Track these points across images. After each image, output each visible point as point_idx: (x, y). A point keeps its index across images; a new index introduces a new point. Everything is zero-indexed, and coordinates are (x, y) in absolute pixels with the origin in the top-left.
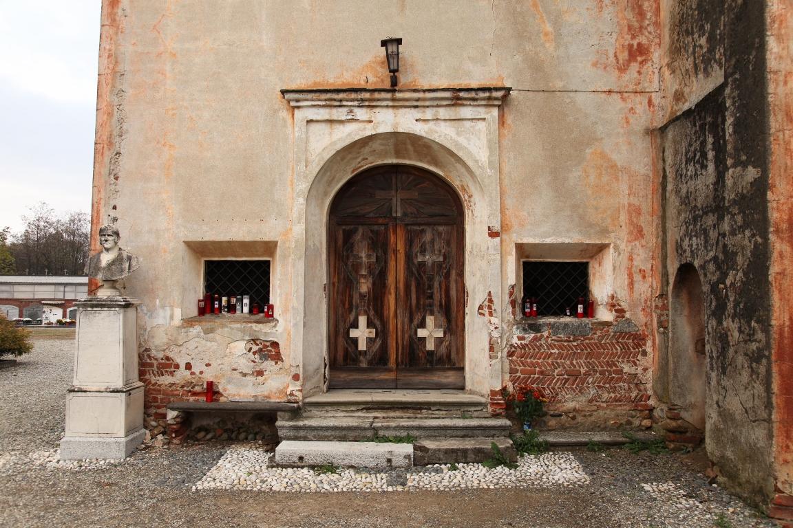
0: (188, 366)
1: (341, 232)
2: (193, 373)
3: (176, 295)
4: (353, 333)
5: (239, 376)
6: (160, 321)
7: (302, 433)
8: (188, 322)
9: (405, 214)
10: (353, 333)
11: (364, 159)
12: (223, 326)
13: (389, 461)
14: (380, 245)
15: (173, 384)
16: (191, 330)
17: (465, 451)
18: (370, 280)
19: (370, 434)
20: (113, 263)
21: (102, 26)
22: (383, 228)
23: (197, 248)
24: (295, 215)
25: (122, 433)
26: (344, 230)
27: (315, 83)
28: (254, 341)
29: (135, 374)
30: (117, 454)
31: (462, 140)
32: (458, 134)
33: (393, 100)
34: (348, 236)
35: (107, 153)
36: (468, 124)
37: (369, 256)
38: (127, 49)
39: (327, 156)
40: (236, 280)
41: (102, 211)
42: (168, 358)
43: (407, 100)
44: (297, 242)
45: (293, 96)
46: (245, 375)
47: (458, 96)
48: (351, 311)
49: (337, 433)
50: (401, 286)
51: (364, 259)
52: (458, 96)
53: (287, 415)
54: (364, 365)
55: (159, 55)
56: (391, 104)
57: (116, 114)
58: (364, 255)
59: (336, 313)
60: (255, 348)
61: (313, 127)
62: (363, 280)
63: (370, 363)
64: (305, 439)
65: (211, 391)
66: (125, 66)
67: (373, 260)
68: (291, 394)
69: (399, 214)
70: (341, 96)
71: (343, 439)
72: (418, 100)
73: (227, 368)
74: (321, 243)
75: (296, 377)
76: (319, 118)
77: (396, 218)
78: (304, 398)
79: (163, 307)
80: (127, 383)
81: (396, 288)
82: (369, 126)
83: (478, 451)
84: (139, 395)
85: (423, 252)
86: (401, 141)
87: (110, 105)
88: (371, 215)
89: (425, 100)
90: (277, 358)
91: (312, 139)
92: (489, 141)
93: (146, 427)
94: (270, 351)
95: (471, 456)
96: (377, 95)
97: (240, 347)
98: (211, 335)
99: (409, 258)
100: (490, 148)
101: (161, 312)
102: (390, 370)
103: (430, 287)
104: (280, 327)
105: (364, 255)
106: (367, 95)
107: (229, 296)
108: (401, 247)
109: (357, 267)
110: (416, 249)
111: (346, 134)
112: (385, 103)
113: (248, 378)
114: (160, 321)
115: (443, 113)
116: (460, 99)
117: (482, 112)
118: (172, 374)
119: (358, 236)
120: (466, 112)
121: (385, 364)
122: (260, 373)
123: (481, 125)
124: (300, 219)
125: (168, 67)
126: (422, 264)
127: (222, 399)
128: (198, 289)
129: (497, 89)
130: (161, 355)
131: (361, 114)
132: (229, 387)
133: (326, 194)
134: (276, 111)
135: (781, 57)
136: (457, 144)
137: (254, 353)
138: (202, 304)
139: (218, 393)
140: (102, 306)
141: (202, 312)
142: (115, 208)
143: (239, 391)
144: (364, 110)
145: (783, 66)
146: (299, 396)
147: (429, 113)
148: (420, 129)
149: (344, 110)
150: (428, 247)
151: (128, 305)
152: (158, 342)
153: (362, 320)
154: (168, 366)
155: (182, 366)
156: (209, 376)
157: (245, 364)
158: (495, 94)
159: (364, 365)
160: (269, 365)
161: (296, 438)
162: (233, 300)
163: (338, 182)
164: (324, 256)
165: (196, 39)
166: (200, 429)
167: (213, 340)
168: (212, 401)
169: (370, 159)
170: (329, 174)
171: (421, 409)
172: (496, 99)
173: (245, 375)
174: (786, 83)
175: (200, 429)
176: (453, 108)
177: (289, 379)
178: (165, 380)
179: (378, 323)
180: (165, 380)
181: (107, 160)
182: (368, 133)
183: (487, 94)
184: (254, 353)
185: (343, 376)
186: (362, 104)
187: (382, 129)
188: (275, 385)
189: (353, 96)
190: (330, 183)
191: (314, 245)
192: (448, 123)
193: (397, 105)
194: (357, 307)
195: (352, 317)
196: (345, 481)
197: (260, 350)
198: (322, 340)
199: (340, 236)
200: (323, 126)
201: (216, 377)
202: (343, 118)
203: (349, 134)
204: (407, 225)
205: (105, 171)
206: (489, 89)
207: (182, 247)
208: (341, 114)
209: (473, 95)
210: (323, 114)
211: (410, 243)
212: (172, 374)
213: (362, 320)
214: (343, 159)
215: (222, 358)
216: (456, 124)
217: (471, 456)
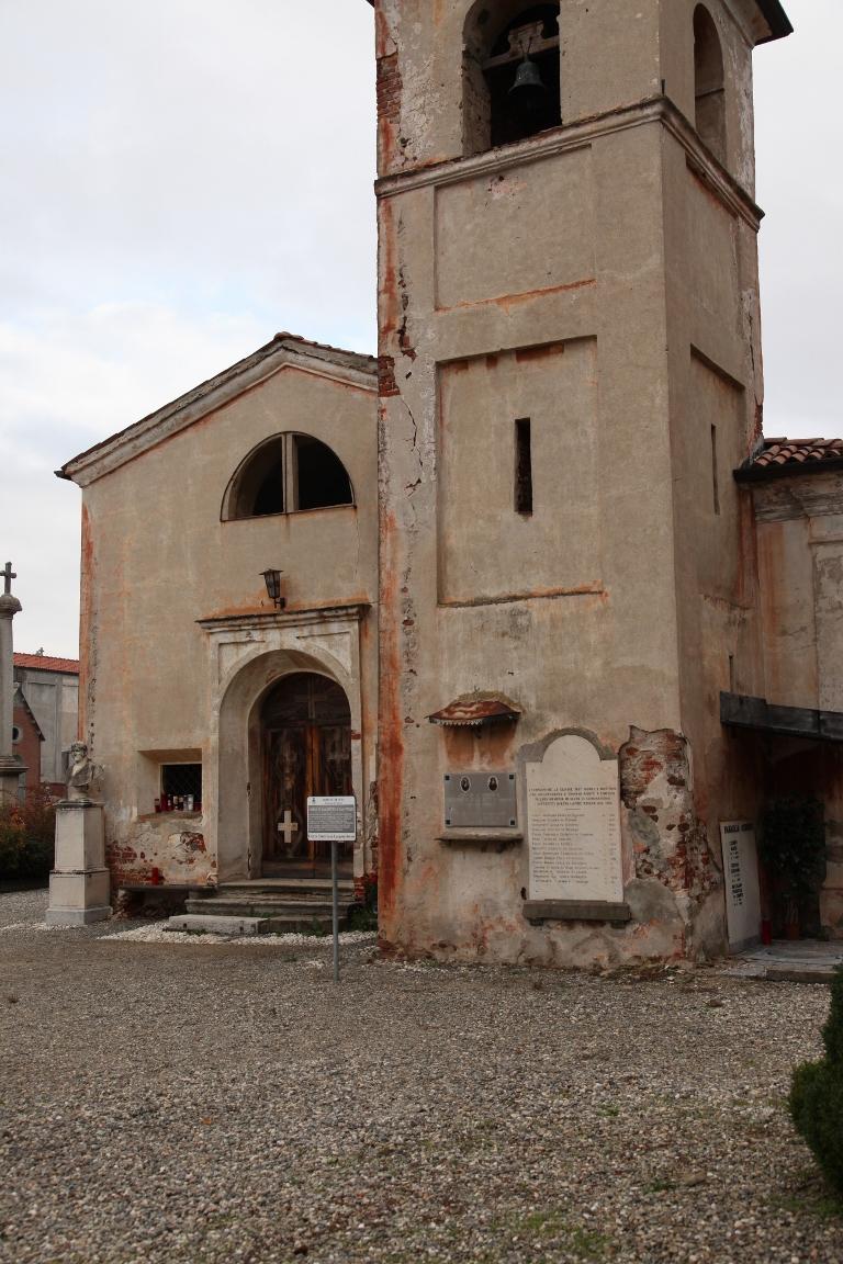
0: (143, 855)
1: (270, 735)
2: (145, 861)
3: (134, 797)
4: (281, 827)
5: (176, 863)
6: (123, 817)
7: (202, 909)
8: (142, 818)
9: (319, 716)
10: (281, 827)
11: (272, 671)
12: (164, 821)
13: (242, 929)
14: (300, 746)
15: (133, 870)
16: (143, 825)
17: (294, 923)
18: (294, 776)
19: (248, 910)
20: (80, 772)
21: (82, 574)
22: (302, 730)
23: (151, 756)
24: (212, 727)
25: (83, 906)
26: (272, 734)
27: (226, 611)
28: (187, 833)
29: (101, 860)
30: (79, 922)
31: (333, 653)
32: (330, 648)
33: (277, 622)
34: (275, 737)
35: (86, 680)
36: (337, 637)
37: (291, 756)
38: (99, 592)
39: (233, 673)
40: (179, 780)
41: (85, 727)
42: (130, 849)
43: (287, 621)
44: (213, 749)
45: (209, 622)
46: (181, 863)
47: (324, 615)
48: (279, 806)
49: (225, 909)
50: (317, 783)
51: (287, 759)
52: (324, 615)
53: (196, 894)
54: (290, 856)
55: (120, 595)
56: (275, 625)
57: (92, 649)
58: (287, 755)
59: (267, 808)
60: (188, 840)
61: (225, 649)
62: (288, 779)
63: (295, 854)
64: (204, 913)
65: (157, 875)
66: (98, 607)
67: (295, 759)
68: (210, 879)
69: (314, 716)
70: (238, 622)
71: (230, 914)
72: (294, 621)
73: (168, 857)
74: (243, 748)
75: (213, 865)
76: (227, 641)
77: (311, 720)
78: (219, 882)
79: (125, 806)
80: (89, 866)
81: (313, 785)
82: (263, 646)
83: (304, 923)
84: (103, 881)
85: (333, 750)
86: (295, 656)
87: (88, 640)
88: (293, 718)
89: (300, 620)
90: (203, 848)
91: (224, 659)
92: (352, 653)
93: (111, 904)
94: (196, 842)
95: (299, 928)
96: (263, 620)
97: (177, 838)
98: (156, 830)
99: (323, 756)
100: (352, 659)
101: (124, 811)
102: (309, 861)
103: (341, 783)
104: (204, 823)
105: (287, 755)
106: (256, 620)
107: (179, 795)
108: (315, 747)
109: (282, 767)
110: (329, 748)
111: (248, 652)
112: (271, 625)
113: (184, 865)
114: (123, 817)
115: (317, 629)
116: (325, 617)
117: (346, 627)
118: (132, 861)
119: (283, 739)
120: (334, 627)
121: (307, 855)
122: (191, 861)
123: (347, 638)
124: (215, 729)
125: (125, 606)
126: (333, 762)
127: (165, 883)
128: (156, 789)
129: (352, 607)
130: (124, 846)
131: (256, 635)
132: (170, 873)
133: (245, 704)
134: (199, 636)
135: (387, 620)
136: (328, 656)
137: (187, 844)
138: (159, 803)
139: (163, 878)
140: (71, 807)
141: (158, 810)
142: (92, 725)
143: (176, 877)
144: (258, 632)
145: (388, 627)
146: (215, 880)
147: (306, 632)
148: (299, 646)
149: (245, 633)
150: (337, 745)
151: (88, 806)
152: (122, 834)
153: (288, 815)
154: (129, 855)
155: (139, 855)
156: (156, 864)
157: (180, 853)
158: (350, 611)
159: (290, 856)
160: (197, 853)
161: (199, 913)
162: (181, 799)
163: (255, 691)
164: (246, 760)
165: (143, 578)
166: (148, 908)
167: (158, 833)
168: (157, 884)
169: (279, 670)
170: (241, 687)
171: (305, 893)
172: (353, 614)
173: (181, 863)
174: (390, 639)
175: (148, 908)
176: (323, 625)
177: (209, 865)
178: (128, 867)
179: (299, 817)
180: (128, 867)
181: (87, 685)
182: (262, 652)
183: (344, 612)
184: (187, 844)
185: (273, 866)
186: (255, 627)
187: (272, 648)
188: (201, 872)
189: (247, 621)
190: (247, 694)
191: (233, 750)
192: (322, 638)
193: (281, 626)
194: (284, 803)
195: (280, 812)
196: (210, 939)
197: (191, 842)
198: (245, 834)
199: (270, 739)
200: (232, 647)
201: (161, 864)
202: (244, 640)
203: (248, 654)
204: (320, 727)
205: (85, 695)
206: (345, 608)
207: (138, 755)
208: (242, 637)
209: (333, 613)
210: (229, 637)
211: (323, 743)
212: (132, 861)
213: (288, 815)
214: (251, 674)
215: (163, 849)
216: (327, 638)
217: (299, 928)
